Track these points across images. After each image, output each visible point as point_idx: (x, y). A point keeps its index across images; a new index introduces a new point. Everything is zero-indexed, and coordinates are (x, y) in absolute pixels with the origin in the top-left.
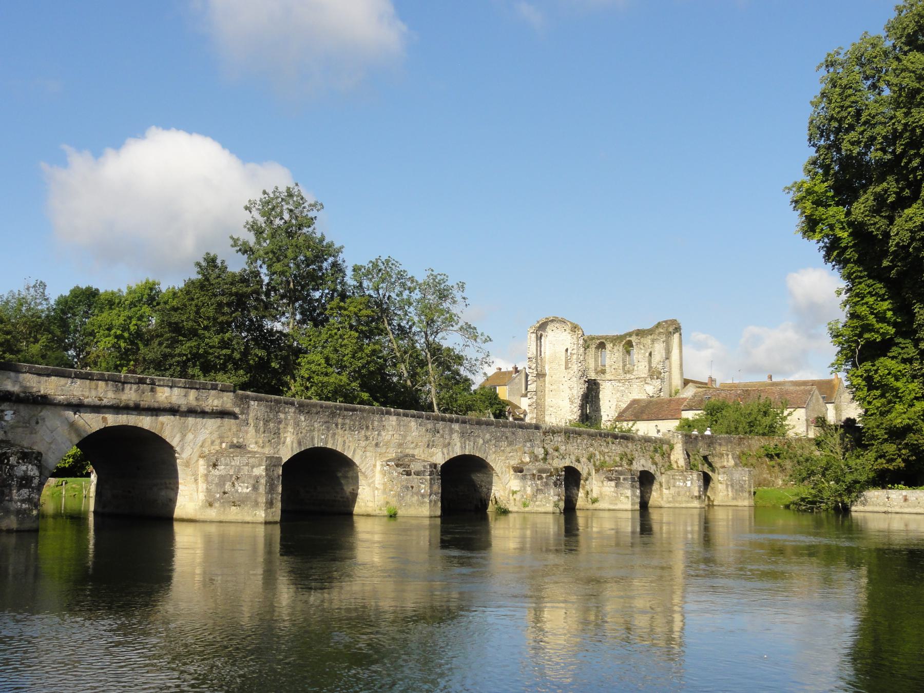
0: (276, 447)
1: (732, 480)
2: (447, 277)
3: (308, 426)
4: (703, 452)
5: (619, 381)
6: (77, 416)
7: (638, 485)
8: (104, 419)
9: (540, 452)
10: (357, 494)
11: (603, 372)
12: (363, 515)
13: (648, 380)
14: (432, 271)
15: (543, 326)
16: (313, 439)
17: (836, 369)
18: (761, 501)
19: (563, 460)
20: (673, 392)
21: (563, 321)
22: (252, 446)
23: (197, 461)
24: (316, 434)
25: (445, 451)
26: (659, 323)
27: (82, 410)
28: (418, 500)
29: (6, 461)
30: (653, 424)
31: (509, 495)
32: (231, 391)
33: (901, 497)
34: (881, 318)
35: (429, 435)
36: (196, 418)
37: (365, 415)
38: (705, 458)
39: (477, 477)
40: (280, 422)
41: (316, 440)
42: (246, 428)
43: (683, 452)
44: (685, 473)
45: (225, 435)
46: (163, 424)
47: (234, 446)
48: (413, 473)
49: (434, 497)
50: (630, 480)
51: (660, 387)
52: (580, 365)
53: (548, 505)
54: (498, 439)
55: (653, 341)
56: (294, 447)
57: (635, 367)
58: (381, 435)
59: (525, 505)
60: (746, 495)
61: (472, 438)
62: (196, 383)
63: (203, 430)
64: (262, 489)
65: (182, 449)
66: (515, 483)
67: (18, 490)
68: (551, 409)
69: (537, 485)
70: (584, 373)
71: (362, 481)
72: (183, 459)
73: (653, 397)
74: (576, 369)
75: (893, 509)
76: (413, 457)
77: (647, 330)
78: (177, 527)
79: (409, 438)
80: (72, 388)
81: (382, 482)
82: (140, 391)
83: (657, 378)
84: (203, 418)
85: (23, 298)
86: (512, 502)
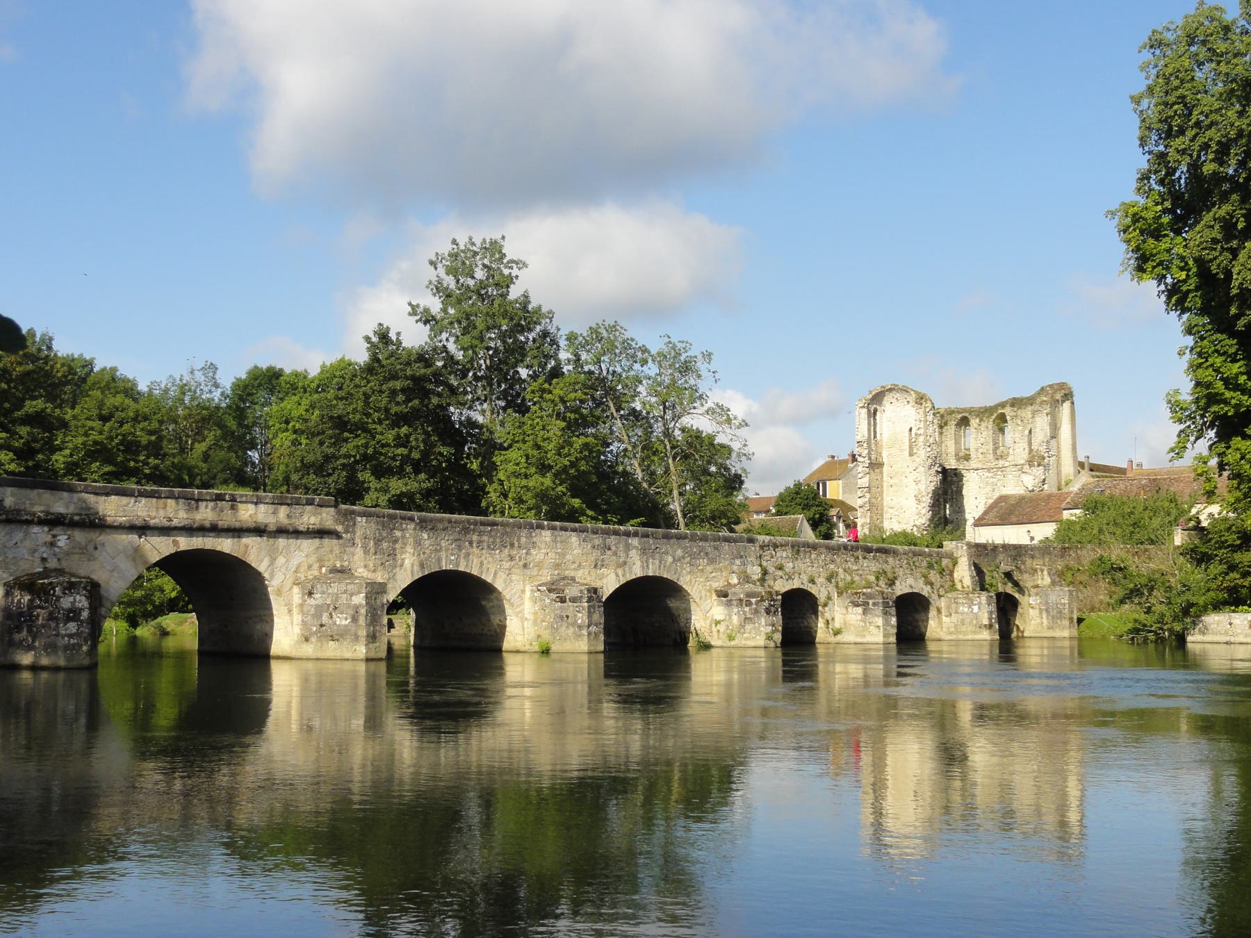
0: (391, 571)
1: (1047, 603)
2: (691, 345)
3: (433, 545)
4: (1004, 567)
5: (989, 470)
6: (142, 540)
7: (893, 611)
8: (176, 543)
9: (755, 572)
10: (505, 627)
11: (967, 458)
12: (512, 652)
13: (1026, 468)
14: (669, 337)
15: (878, 398)
16: (439, 560)
17: (1178, 454)
18: (1087, 631)
19: (790, 581)
20: (1063, 483)
21: (905, 390)
22: (360, 570)
23: (291, 588)
24: (443, 555)
25: (620, 572)
26: (1042, 389)
27: (148, 532)
28: (574, 633)
29: (52, 592)
30: (1023, 529)
31: (711, 625)
32: (331, 506)
33: (1246, 622)
34: (1230, 383)
35: (597, 553)
36: (288, 538)
37: (508, 530)
38: (1008, 575)
39: (673, 604)
40: (396, 541)
41: (444, 561)
42: (352, 549)
43: (970, 568)
44: (971, 595)
45: (326, 558)
46: (247, 546)
47: (334, 570)
48: (568, 600)
49: (593, 629)
50: (881, 605)
51: (1043, 477)
52: (929, 449)
53: (758, 637)
54: (693, 556)
55: (1034, 413)
56: (415, 570)
57: (1011, 450)
58: (531, 554)
59: (731, 638)
60: (1066, 623)
61: (657, 556)
62: (287, 497)
63: (297, 552)
64: (362, 621)
65: (272, 575)
66: (718, 611)
67: (65, 624)
68: (891, 511)
69: (745, 613)
70: (935, 460)
71: (509, 611)
72: (273, 586)
73: (1033, 491)
74: (923, 455)
75: (1236, 638)
76: (571, 580)
77: (1026, 398)
78: (274, 665)
79: (569, 557)
80: (135, 508)
81: (533, 611)
82: (218, 509)
83: (1039, 465)
84: (297, 538)
85: (185, 385)
86: (715, 634)
